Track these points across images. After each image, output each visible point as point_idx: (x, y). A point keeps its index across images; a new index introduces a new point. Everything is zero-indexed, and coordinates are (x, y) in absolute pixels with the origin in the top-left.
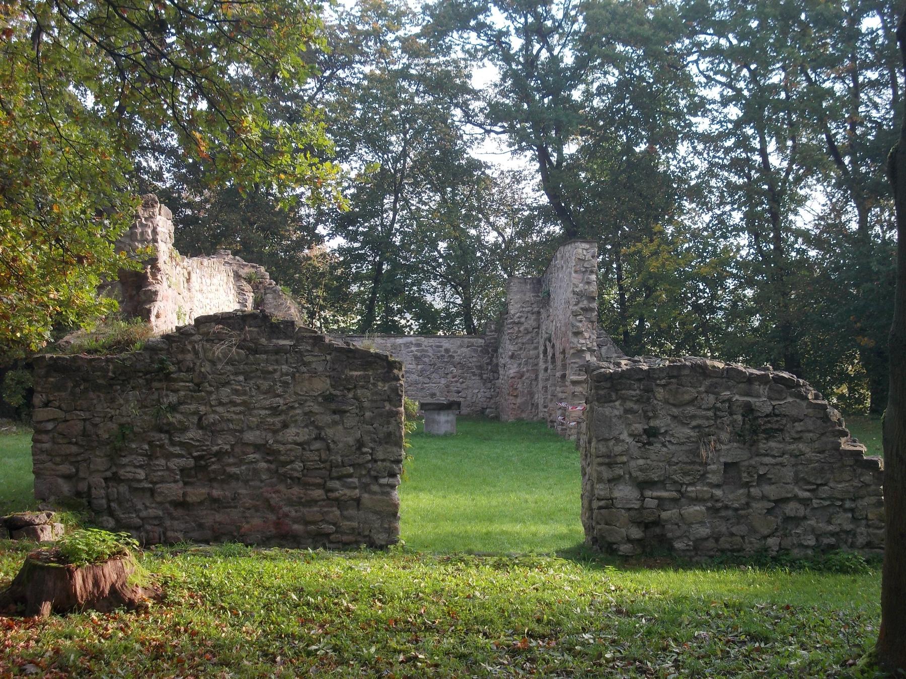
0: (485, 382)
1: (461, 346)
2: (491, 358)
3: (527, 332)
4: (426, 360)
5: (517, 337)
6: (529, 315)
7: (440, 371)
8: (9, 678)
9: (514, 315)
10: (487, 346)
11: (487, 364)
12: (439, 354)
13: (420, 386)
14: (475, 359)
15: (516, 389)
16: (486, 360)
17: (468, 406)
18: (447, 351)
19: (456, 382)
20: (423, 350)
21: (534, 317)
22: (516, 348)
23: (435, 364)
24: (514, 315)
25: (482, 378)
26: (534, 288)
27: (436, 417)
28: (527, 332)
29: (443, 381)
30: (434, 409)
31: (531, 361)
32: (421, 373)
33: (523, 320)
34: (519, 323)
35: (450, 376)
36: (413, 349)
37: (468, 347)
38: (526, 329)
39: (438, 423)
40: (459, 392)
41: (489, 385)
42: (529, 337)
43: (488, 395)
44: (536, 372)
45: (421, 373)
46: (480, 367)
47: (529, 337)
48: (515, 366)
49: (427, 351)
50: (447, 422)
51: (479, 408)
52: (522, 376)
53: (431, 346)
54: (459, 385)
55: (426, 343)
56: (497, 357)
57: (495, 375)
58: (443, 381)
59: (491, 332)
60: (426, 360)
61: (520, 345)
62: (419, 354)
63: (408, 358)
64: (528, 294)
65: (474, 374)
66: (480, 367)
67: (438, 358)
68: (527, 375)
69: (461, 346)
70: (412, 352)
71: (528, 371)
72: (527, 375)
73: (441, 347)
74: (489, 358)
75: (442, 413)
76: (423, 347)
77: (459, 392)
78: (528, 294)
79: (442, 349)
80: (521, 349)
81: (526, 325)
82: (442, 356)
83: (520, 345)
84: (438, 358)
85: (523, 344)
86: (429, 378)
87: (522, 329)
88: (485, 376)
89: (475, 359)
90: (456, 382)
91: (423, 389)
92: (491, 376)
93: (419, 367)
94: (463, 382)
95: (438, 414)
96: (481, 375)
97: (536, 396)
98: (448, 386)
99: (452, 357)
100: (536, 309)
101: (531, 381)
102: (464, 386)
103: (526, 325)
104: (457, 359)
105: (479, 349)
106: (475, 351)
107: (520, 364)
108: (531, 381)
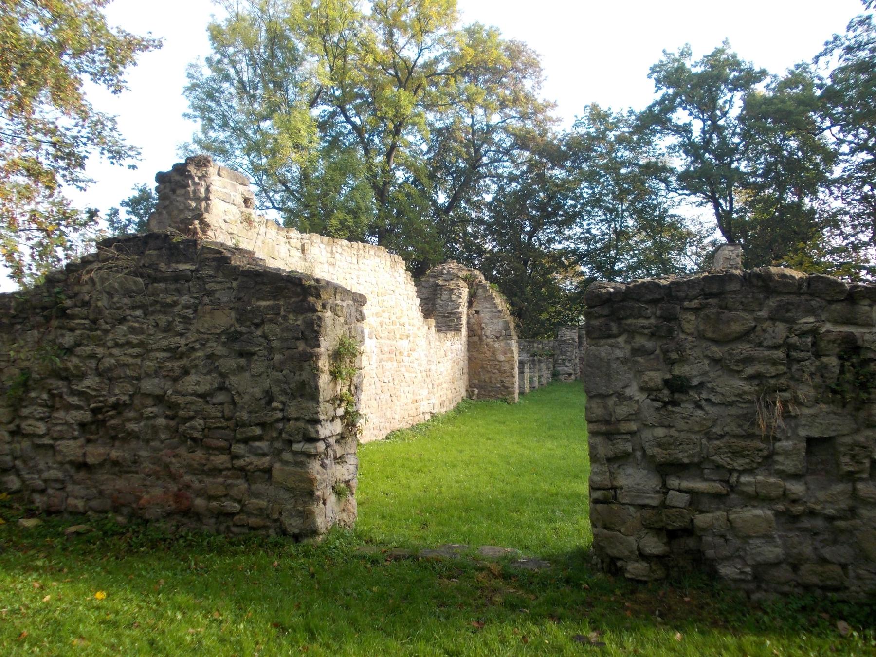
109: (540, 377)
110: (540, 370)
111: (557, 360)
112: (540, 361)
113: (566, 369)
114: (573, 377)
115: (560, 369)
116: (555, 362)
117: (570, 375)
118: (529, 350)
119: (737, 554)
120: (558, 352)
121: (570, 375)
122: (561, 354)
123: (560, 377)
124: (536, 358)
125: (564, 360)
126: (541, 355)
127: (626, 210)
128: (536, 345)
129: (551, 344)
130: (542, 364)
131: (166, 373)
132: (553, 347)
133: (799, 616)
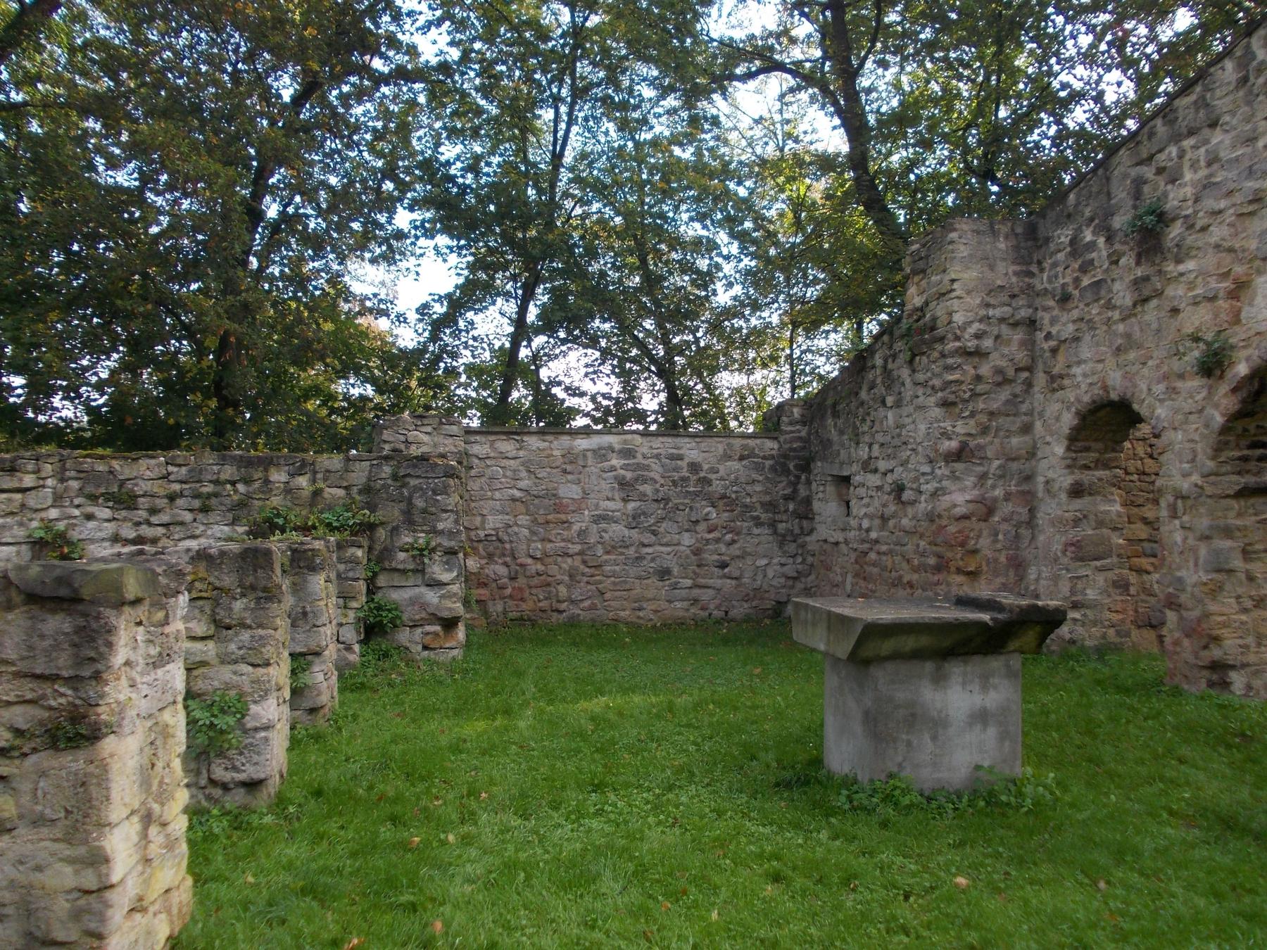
0: (782, 540)
1: (727, 457)
2: (794, 485)
3: (1003, 380)
4: (647, 489)
5: (975, 395)
6: (1005, 329)
7: (681, 517)
8: (926, 2)
9: (963, 328)
10: (785, 456)
11: (787, 498)
12: (676, 476)
13: (631, 552)
14: (758, 488)
15: (975, 552)
16: (782, 489)
17: (746, 598)
18: (694, 467)
19: (718, 540)
20: (639, 467)
21: (1018, 336)
22: (971, 426)
23: (666, 500)
24: (963, 328)
25: (775, 532)
26: (1016, 248)
27: (929, 696)
28: (1003, 380)
29: (687, 539)
30: (917, 655)
31: (1014, 466)
32: (635, 521)
33: (988, 343)
34: (979, 354)
35: (702, 527)
36: (615, 462)
37: (742, 458)
38: (999, 371)
39: (938, 725)
40: (723, 565)
41: (792, 548)
42: (1004, 394)
43: (790, 570)
44: (1028, 497)
45: (635, 521)
46: (770, 506)
47: (1004, 394)
48: (970, 481)
49: (647, 468)
50: (981, 717)
51: (769, 604)
52: (990, 511)
53: (658, 456)
54: (723, 548)
55: (645, 450)
56: (809, 483)
57: (805, 523)
58: (687, 539)
59: (791, 424)
60: (647, 489)
61: (983, 418)
62: (629, 475)
63: (604, 485)
64: (1001, 267)
65: (758, 523)
66: (770, 506)
67: (674, 483)
68: (1006, 508)
69: (727, 457)
70: (613, 469)
71: (1007, 497)
72: (1006, 508)
73: (681, 458)
74: (790, 483)
75: (956, 670)
76: (639, 459)
77: (723, 565)
78: (1001, 267)
79: (683, 464)
80: (985, 431)
81: (996, 360)
82: (683, 479)
83: (983, 418)
84: (674, 483)
85: (992, 414)
86: (654, 533)
87: (985, 370)
88: (781, 527)
89: (758, 488)
90: (718, 540)
91: (640, 558)
92: (795, 525)
93: (631, 505)
94: (734, 542)
95: (939, 680)
96: (773, 525)
97: (1032, 573)
98: (697, 552)
99: (706, 481)
100: (1024, 313)
101: (1018, 526)
102: (735, 550)
103: (996, 360)
104: (717, 487)
105: (768, 463)
106: (759, 468)
107: (983, 477)
108: (1018, 526)
109: (301, 660)
110: (302, 618)
111: (387, 553)
112: (302, 562)
113: (431, 596)
114: (461, 633)
115: (401, 595)
116: (380, 560)
117: (449, 624)
118: (242, 504)
119: (1238, 52)
120: (391, 513)
121: (449, 624)
122: (410, 521)
123: (404, 636)
124: (276, 544)
125: (420, 553)
126: (306, 529)
127: (298, 308)
128: (278, 476)
129: (359, 474)
130: (319, 583)
131: (1148, 598)
132: (367, 490)
133: (1167, 843)
